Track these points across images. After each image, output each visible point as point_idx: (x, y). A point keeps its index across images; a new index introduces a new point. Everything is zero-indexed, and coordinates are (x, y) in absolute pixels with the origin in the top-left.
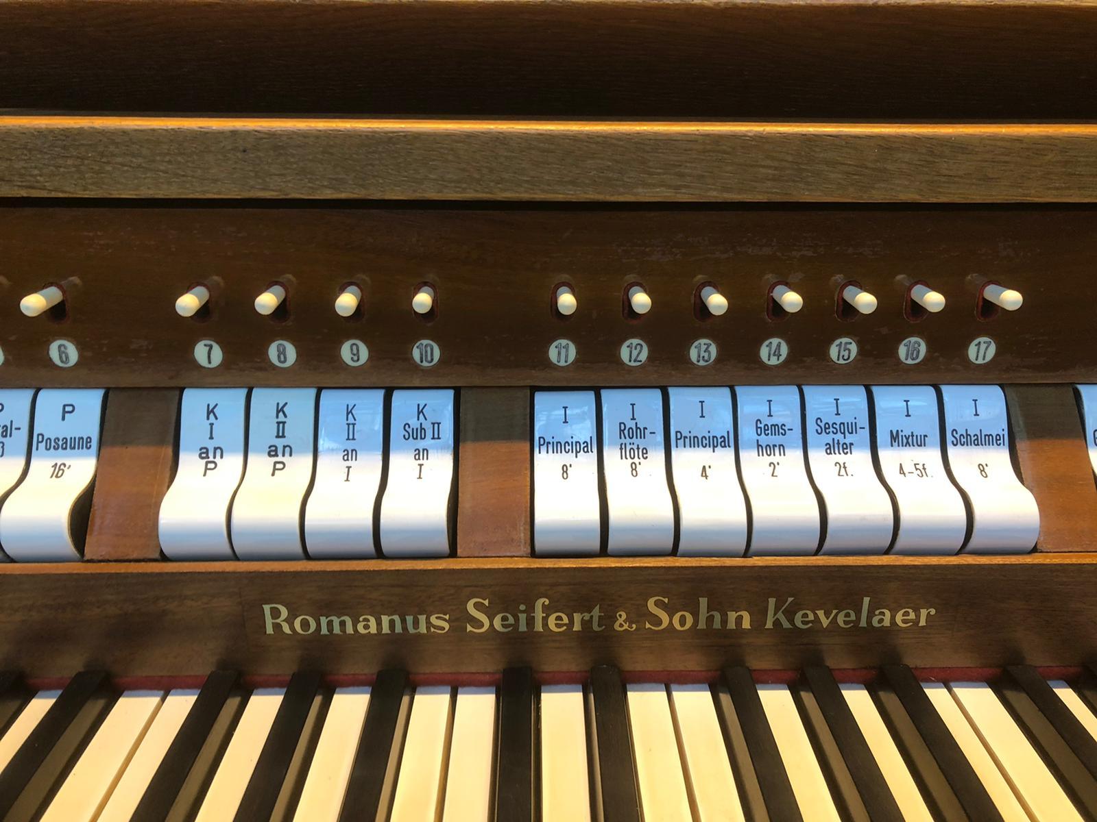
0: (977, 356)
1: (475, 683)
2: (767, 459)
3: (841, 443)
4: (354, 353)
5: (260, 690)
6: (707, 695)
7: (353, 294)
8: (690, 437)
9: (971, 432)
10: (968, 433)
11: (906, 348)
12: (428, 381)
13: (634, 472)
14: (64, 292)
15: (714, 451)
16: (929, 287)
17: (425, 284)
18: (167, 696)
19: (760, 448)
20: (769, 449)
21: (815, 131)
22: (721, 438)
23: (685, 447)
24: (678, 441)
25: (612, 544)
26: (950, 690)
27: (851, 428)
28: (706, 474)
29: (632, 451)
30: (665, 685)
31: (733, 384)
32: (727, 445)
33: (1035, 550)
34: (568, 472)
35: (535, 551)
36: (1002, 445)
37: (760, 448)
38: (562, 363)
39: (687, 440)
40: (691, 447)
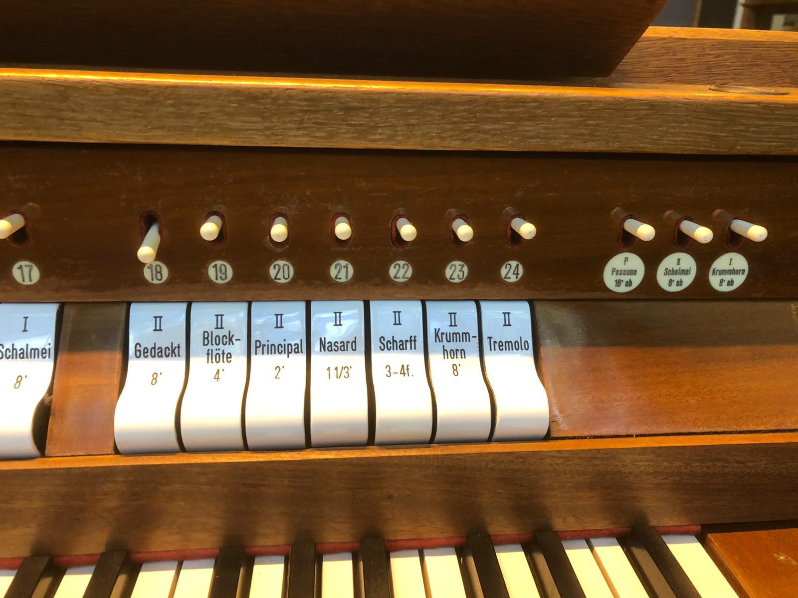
0: (23, 277)
1: (437, 546)
2: (451, 361)
3: (226, 352)
4: (220, 271)
5: (73, 570)
6: (521, 555)
7: (215, 224)
8: (268, 345)
9: (397, 339)
10: (15, 347)
11: (150, 269)
12: (508, 293)
13: (455, 372)
14: (26, 218)
15: (288, 357)
16: (751, 223)
17: (215, 213)
18: (180, 571)
19: (445, 352)
20: (454, 353)
21: (120, 80)
22: (295, 345)
23: (263, 354)
24: (257, 349)
25: (379, 436)
26: (592, 549)
27: (466, 336)
28: (218, 376)
29: (218, 356)
30: (586, 540)
31: (310, 300)
32: (404, 347)
33: (548, 437)
34: (457, 370)
35: (310, 442)
36: (47, 357)
37: (445, 352)
38: (27, 282)
39: (265, 348)
40: (268, 354)
